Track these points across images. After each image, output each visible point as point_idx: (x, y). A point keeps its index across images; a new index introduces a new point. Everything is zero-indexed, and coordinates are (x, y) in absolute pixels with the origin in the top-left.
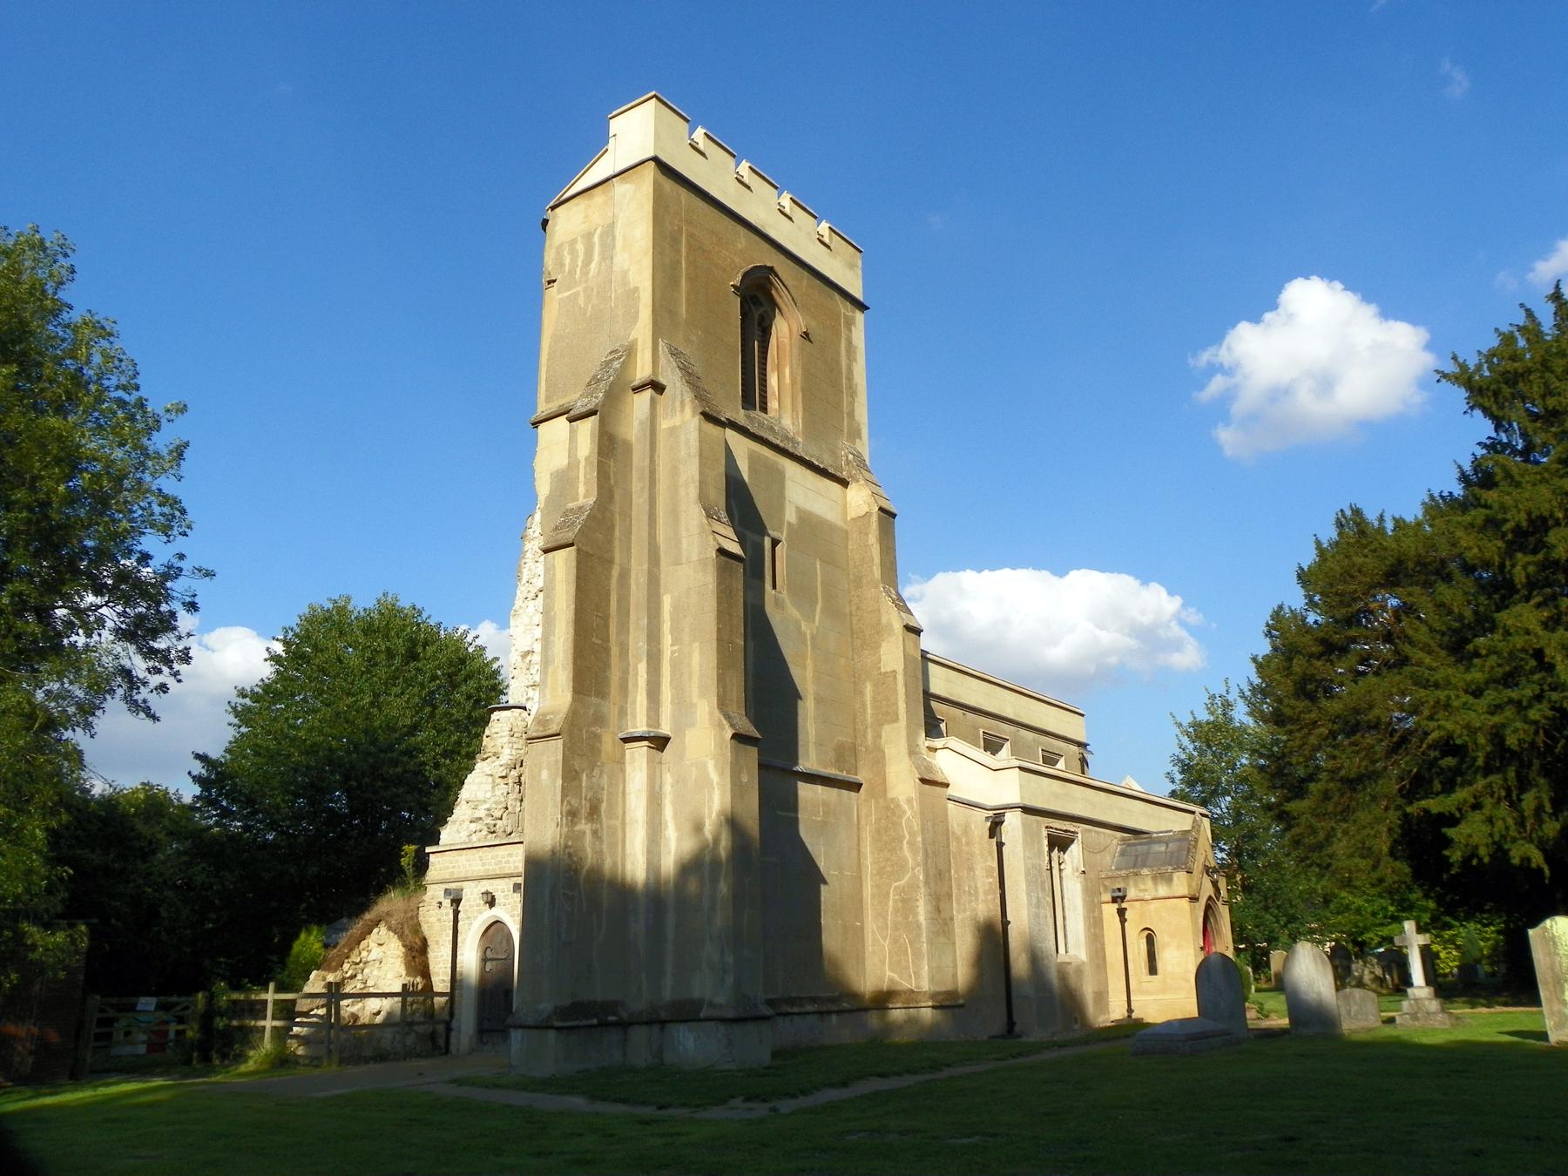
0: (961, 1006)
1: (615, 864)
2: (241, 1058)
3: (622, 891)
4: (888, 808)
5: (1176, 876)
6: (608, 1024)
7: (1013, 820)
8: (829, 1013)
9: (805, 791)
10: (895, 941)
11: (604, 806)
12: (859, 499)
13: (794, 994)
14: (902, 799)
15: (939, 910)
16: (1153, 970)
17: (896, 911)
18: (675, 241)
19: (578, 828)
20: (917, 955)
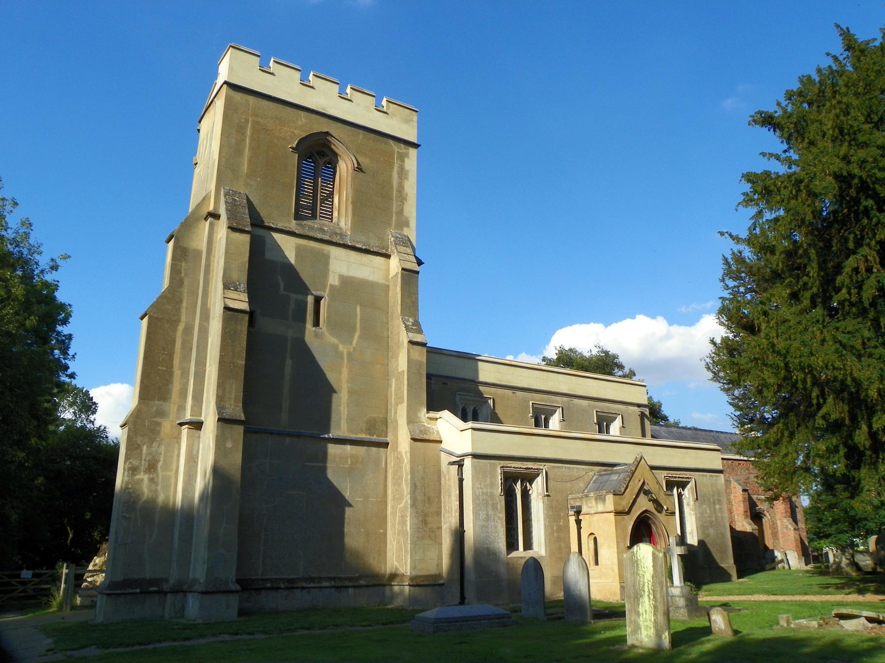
0: (443, 584)
1: (167, 498)
2: (48, 605)
3: (169, 512)
4: (398, 458)
5: (607, 497)
7: (468, 462)
8: (347, 587)
10: (398, 542)
11: (160, 464)
12: (395, 265)
14: (403, 452)
15: (425, 523)
16: (597, 563)
17: (399, 523)
18: (241, 129)
19: (137, 477)
20: (406, 552)
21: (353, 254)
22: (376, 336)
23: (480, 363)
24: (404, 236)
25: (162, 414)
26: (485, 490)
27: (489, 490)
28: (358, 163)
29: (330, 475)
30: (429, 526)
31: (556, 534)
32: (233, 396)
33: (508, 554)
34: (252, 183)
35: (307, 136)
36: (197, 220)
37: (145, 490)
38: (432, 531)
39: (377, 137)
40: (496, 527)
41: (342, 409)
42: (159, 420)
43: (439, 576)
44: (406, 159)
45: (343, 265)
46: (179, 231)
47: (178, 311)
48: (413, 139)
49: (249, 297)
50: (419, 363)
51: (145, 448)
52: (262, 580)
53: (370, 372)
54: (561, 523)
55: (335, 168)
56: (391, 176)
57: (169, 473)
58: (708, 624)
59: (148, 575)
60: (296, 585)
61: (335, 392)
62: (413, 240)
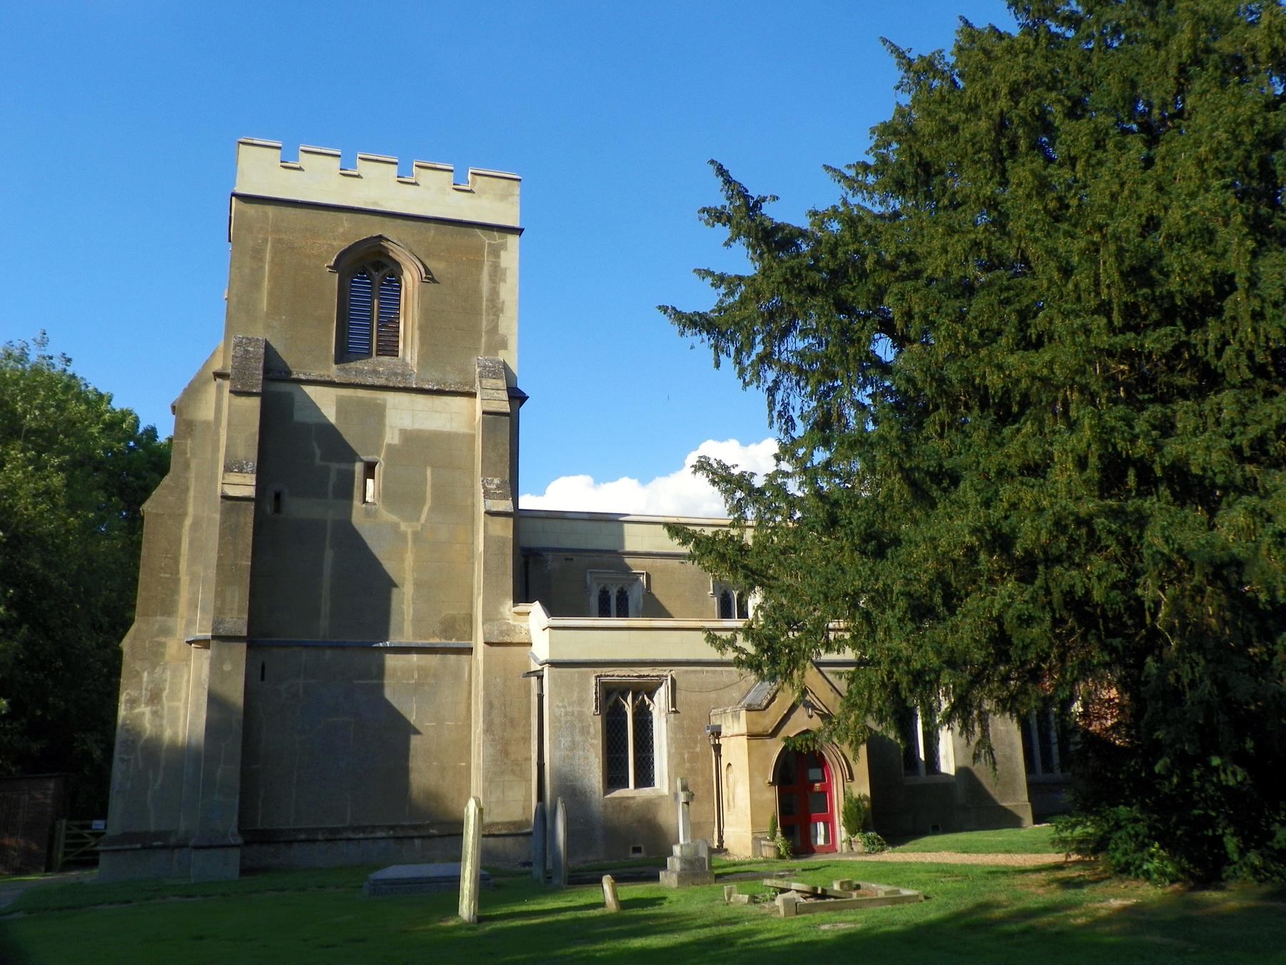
0: (530, 834)
1: (176, 733)
6: (152, 848)
9: (391, 661)
11: (165, 693)
13: (153, 824)
15: (505, 752)
18: (257, 254)
19: (137, 711)
21: (420, 399)
22: (452, 505)
23: (626, 526)
24: (499, 362)
25: (167, 631)
26: (569, 709)
27: (577, 709)
28: (427, 271)
29: (388, 694)
30: (513, 757)
31: (687, 765)
32: (236, 606)
33: (606, 793)
34: (275, 323)
35: (350, 248)
36: (206, 383)
37: (148, 726)
38: (516, 763)
39: (456, 228)
40: (586, 758)
41: (405, 607)
42: (162, 639)
43: (527, 822)
44: (503, 253)
45: (405, 415)
46: (182, 399)
47: (183, 503)
48: (516, 223)
49: (258, 480)
50: (503, 540)
51: (146, 674)
52: (294, 830)
53: (431, 555)
54: (698, 749)
55: (399, 281)
56: (479, 281)
57: (176, 704)
58: (619, 889)
59: (153, 828)
60: (339, 836)
61: (396, 586)
62: (514, 366)
